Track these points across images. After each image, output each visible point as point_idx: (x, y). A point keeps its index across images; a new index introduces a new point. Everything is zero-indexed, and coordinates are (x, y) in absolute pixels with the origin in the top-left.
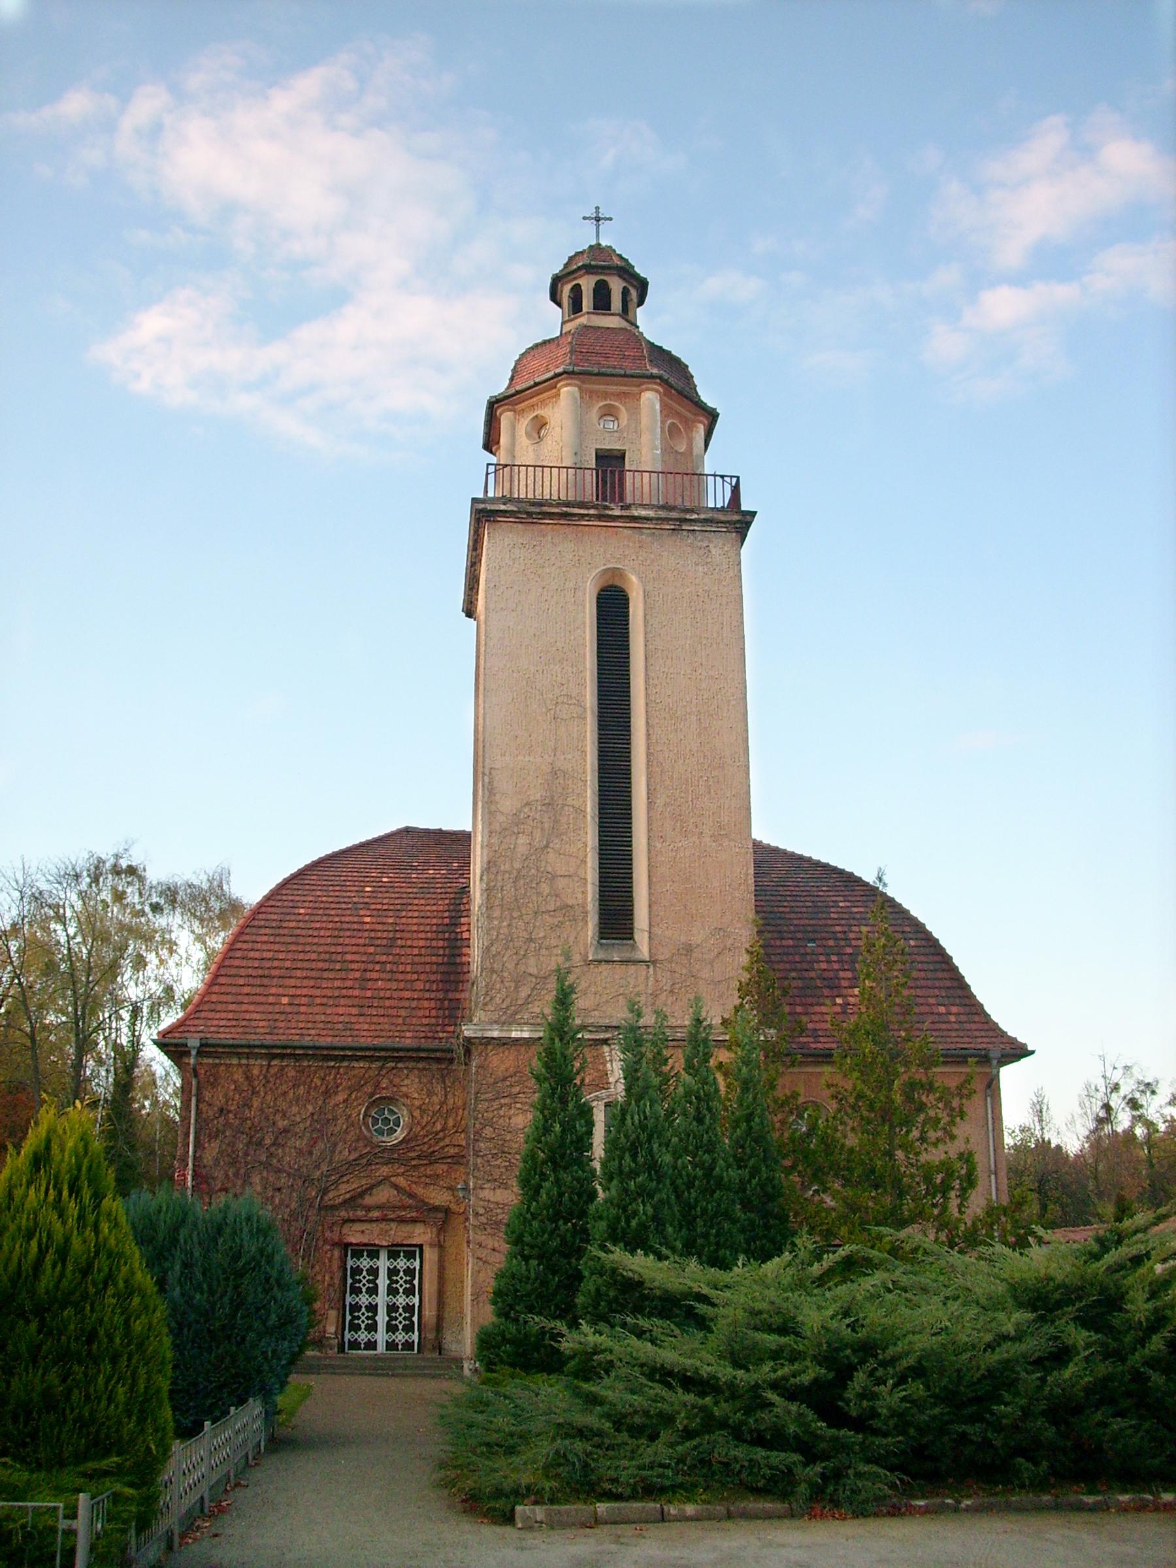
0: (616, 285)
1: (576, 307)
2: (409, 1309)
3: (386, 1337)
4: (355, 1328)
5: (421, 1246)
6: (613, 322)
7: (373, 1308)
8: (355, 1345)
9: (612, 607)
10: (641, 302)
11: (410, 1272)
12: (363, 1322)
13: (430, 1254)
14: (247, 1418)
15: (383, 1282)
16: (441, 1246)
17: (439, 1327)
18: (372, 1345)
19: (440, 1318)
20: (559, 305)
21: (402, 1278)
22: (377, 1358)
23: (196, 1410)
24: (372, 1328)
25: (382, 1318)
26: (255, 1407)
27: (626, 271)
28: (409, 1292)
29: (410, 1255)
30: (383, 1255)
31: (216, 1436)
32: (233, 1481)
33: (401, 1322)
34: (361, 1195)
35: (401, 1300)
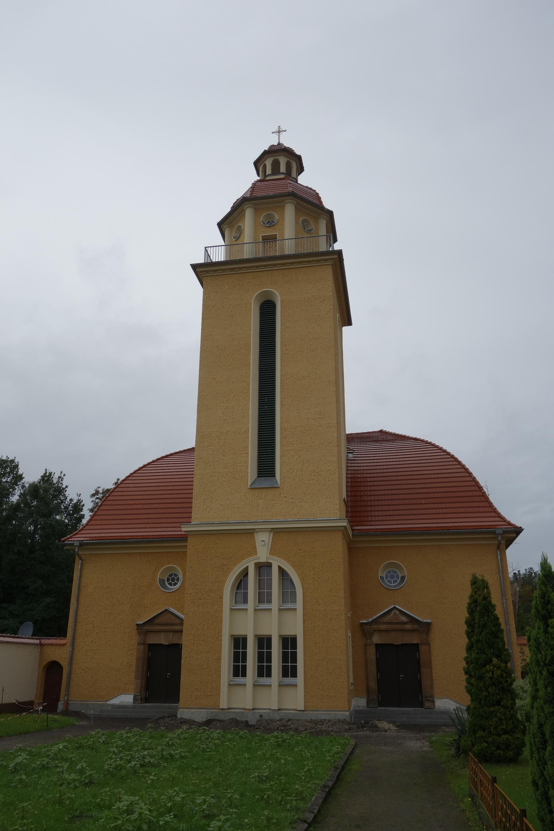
0: (283, 161)
9: (267, 309)
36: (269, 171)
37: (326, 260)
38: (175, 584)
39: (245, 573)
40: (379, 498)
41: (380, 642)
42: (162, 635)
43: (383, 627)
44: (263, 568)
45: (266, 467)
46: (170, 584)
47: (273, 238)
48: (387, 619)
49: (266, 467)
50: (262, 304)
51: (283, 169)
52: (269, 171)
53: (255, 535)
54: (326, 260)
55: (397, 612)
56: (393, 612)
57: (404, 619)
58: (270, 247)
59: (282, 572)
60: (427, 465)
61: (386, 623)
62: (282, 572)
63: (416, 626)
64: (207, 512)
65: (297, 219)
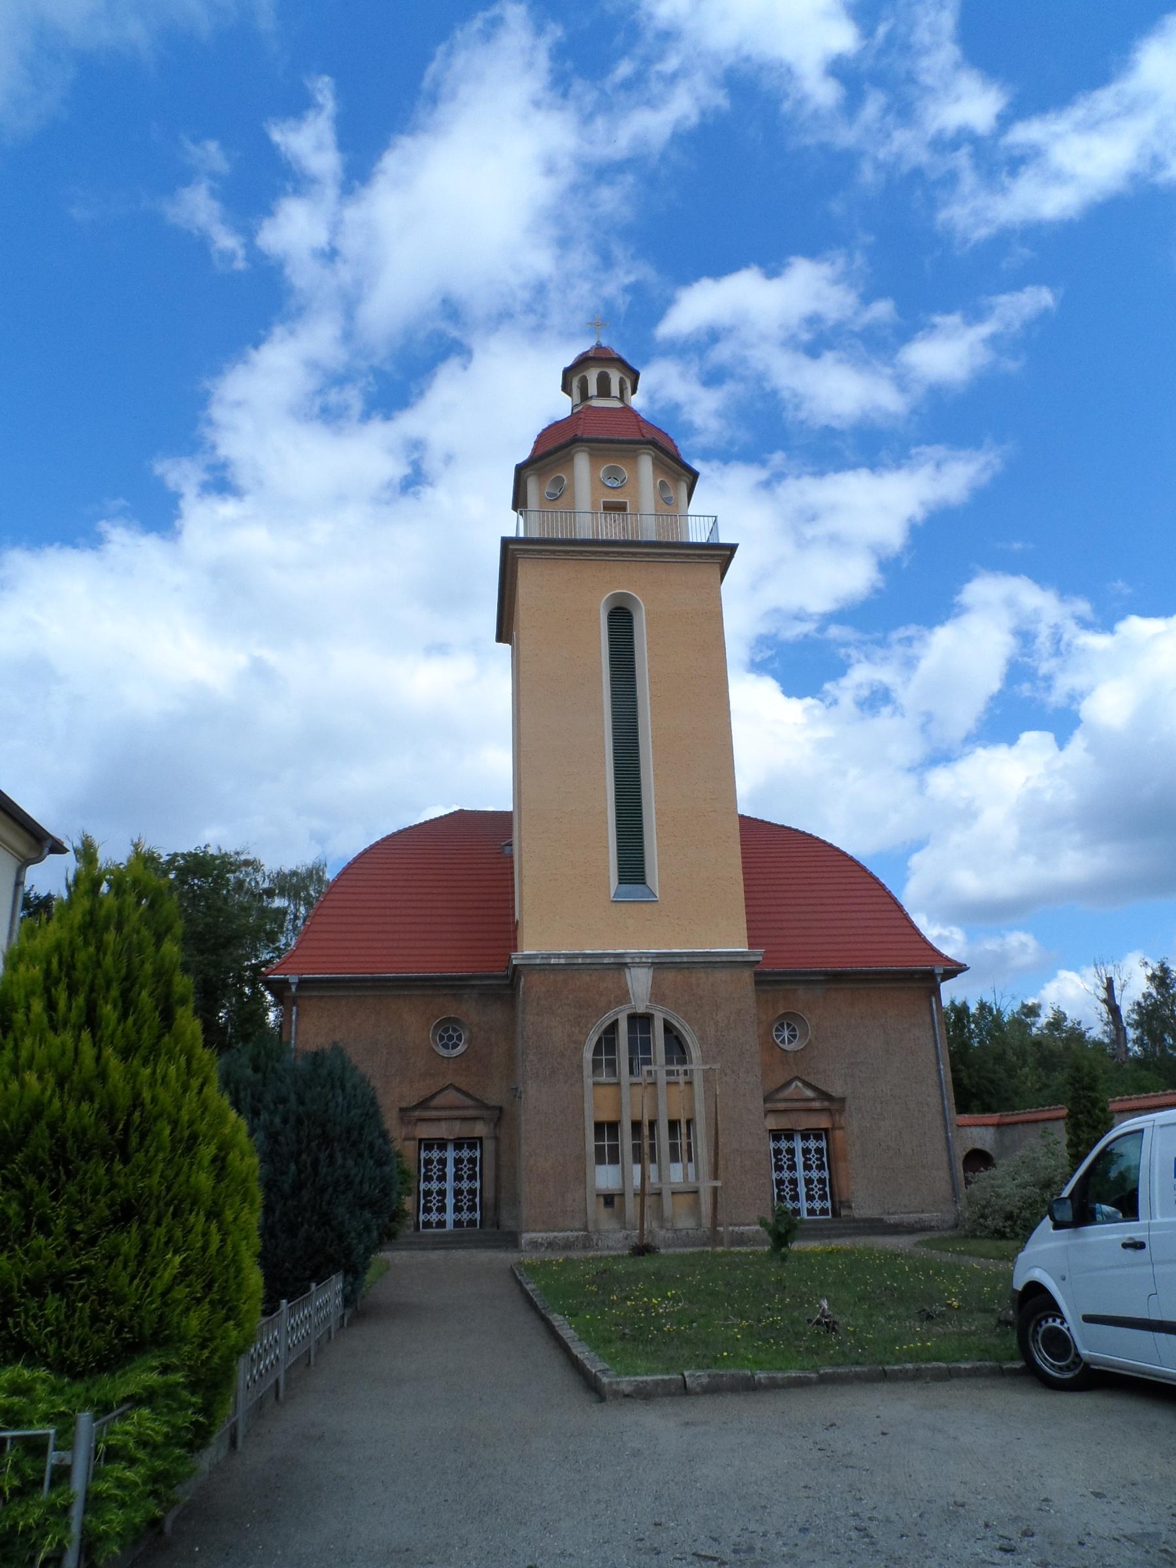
0: (615, 376)
1: (585, 396)
2: (472, 1192)
3: (453, 1217)
4: (428, 1210)
5: (480, 1139)
6: (617, 404)
7: (442, 1193)
8: (427, 1224)
9: (621, 619)
10: (634, 391)
11: (472, 1161)
12: (813, 1156)
13: (489, 1145)
14: (328, 1295)
15: (450, 1170)
16: (497, 1139)
17: (496, 1207)
18: (441, 1224)
19: (497, 1199)
20: (569, 393)
21: (465, 1167)
22: (446, 1235)
23: (285, 1284)
24: (442, 1209)
25: (450, 1201)
26: (337, 1283)
27: (620, 363)
28: (472, 1178)
29: (472, 1147)
30: (450, 1147)
31: (292, 1315)
32: (305, 1361)
33: (465, 1204)
34: (433, 1097)
35: (465, 1185)
36: (593, 389)
37: (712, 556)
38: (455, 1046)
39: (613, 1027)
40: (374, 890)
42: (443, 1125)
43: (781, 1106)
44: (640, 1022)
45: (632, 868)
46: (446, 1046)
47: (620, 507)
49: (632, 868)
51: (615, 390)
52: (593, 389)
53: (627, 971)
54: (712, 556)
55: (800, 1084)
56: (794, 1085)
57: (810, 1093)
59: (668, 1028)
61: (786, 1100)
63: (826, 1104)
64: (546, 931)
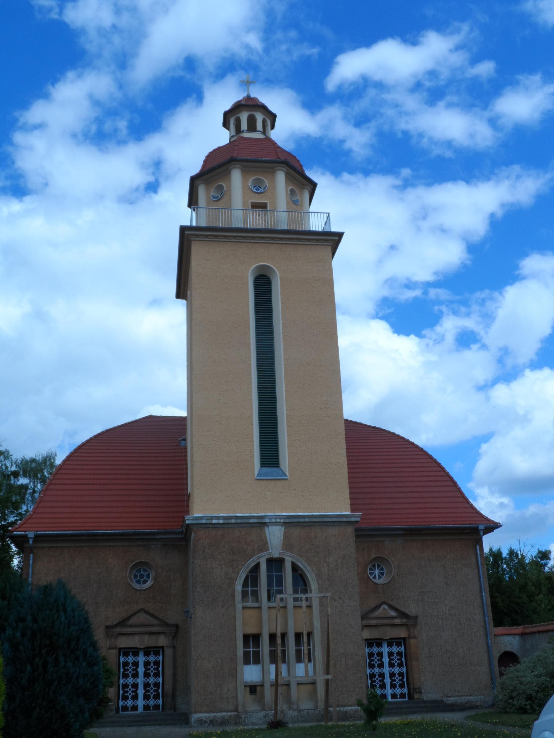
0: (259, 117)
9: (263, 283)
39: (256, 568)
41: (369, 638)
42: (137, 638)
43: (373, 622)
44: (275, 564)
45: (270, 456)
48: (377, 613)
49: (270, 456)
50: (256, 278)
51: (259, 127)
52: (244, 126)
53: (266, 528)
55: (386, 607)
57: (393, 613)
58: (259, 215)
59: (295, 568)
60: (133, 445)
62: (295, 568)
63: (404, 621)
65: (287, 188)
